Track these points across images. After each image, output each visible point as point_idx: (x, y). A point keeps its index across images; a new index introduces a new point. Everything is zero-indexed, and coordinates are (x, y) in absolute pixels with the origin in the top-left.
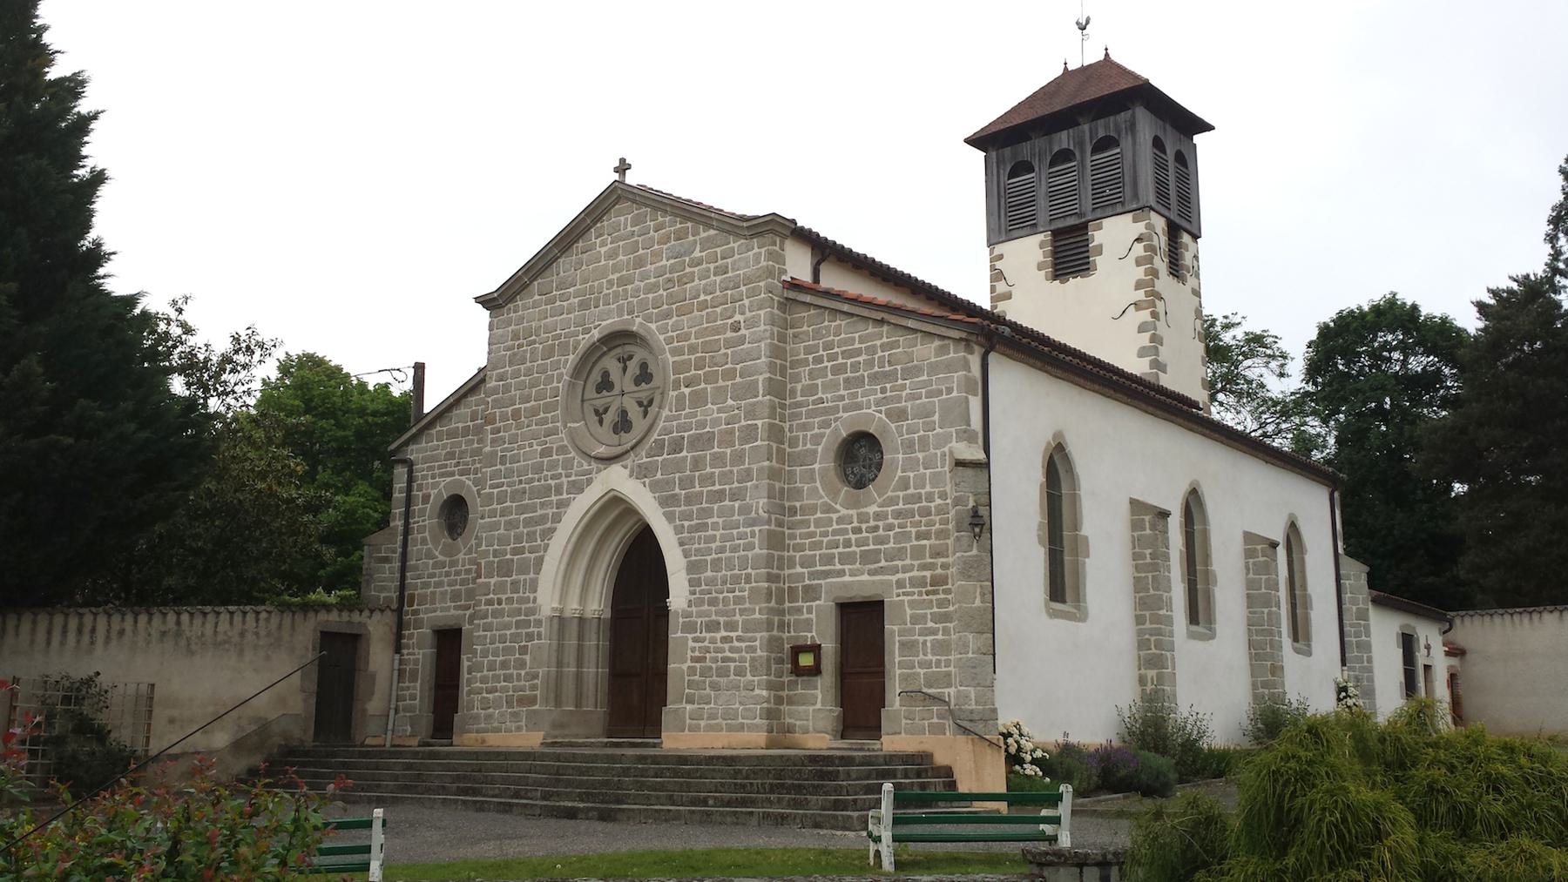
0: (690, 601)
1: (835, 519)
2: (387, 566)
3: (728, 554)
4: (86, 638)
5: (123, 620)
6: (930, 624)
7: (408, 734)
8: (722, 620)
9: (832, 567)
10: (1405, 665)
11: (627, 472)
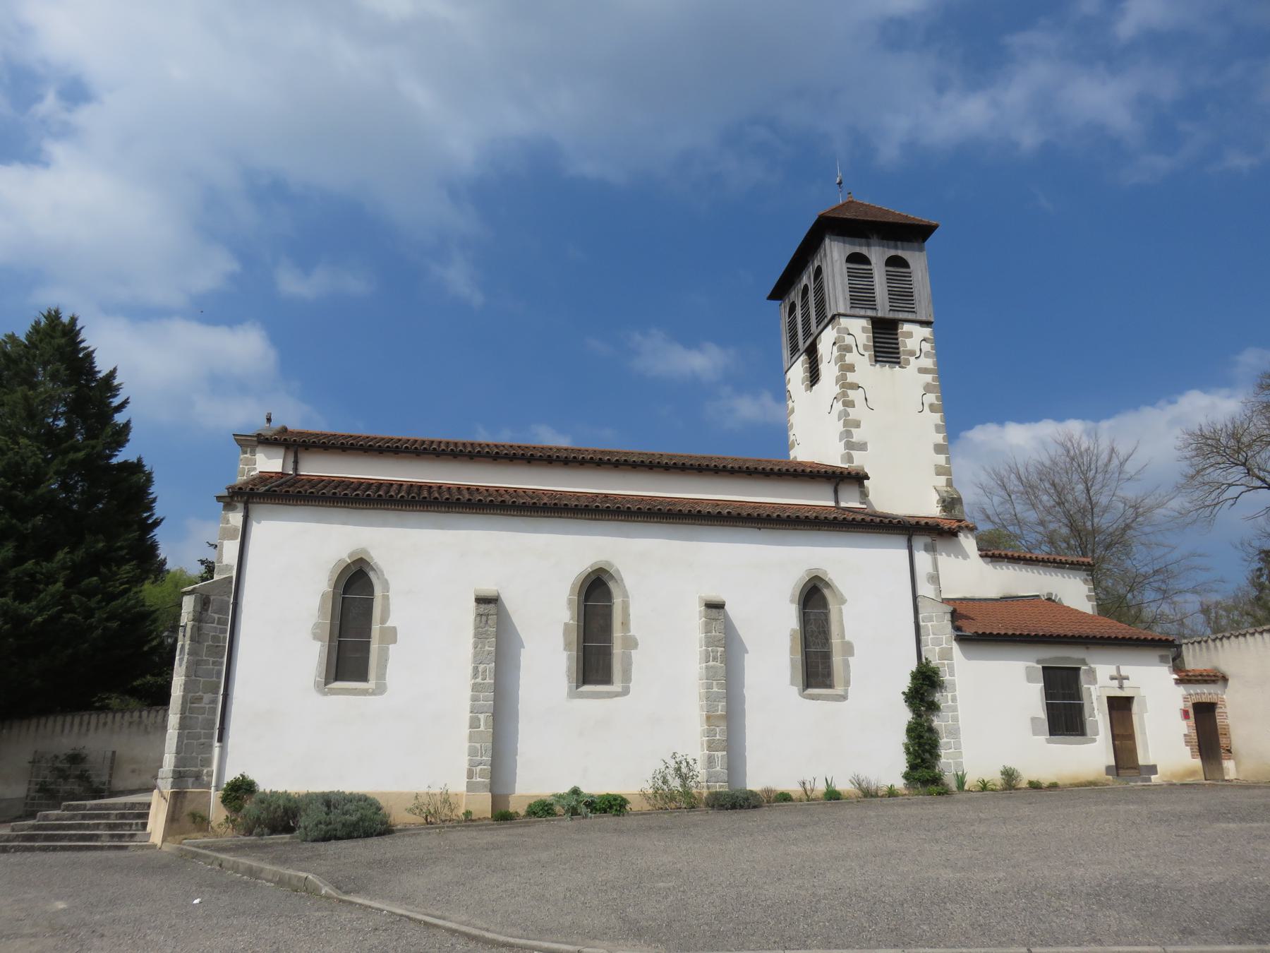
4: (84, 728)
5: (107, 717)
10: (1046, 699)
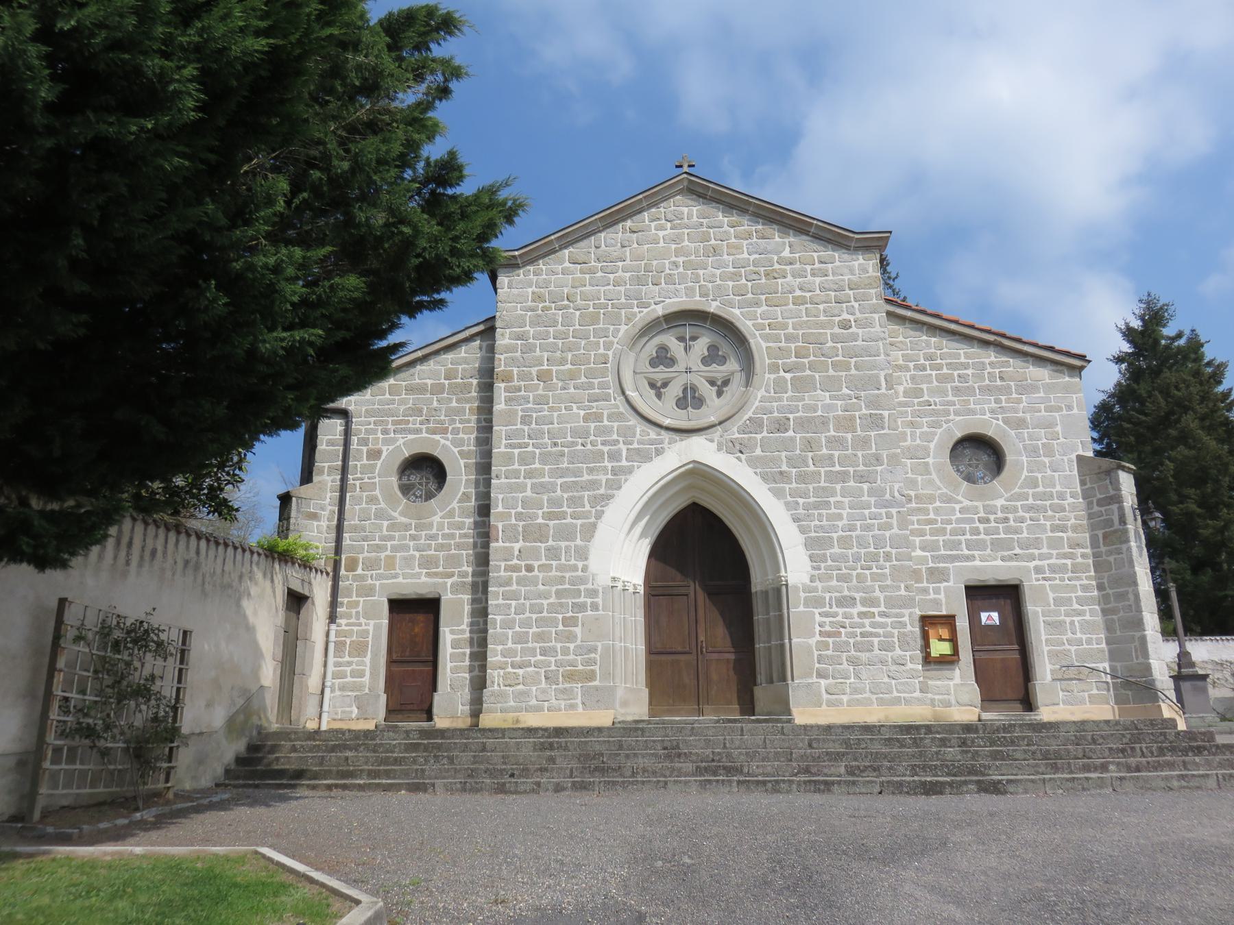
0: (812, 576)
1: (958, 509)
2: (315, 523)
3: (858, 532)
4: (123, 553)
6: (1076, 606)
7: (354, 716)
8: (858, 596)
9: (960, 552)
11: (715, 445)
